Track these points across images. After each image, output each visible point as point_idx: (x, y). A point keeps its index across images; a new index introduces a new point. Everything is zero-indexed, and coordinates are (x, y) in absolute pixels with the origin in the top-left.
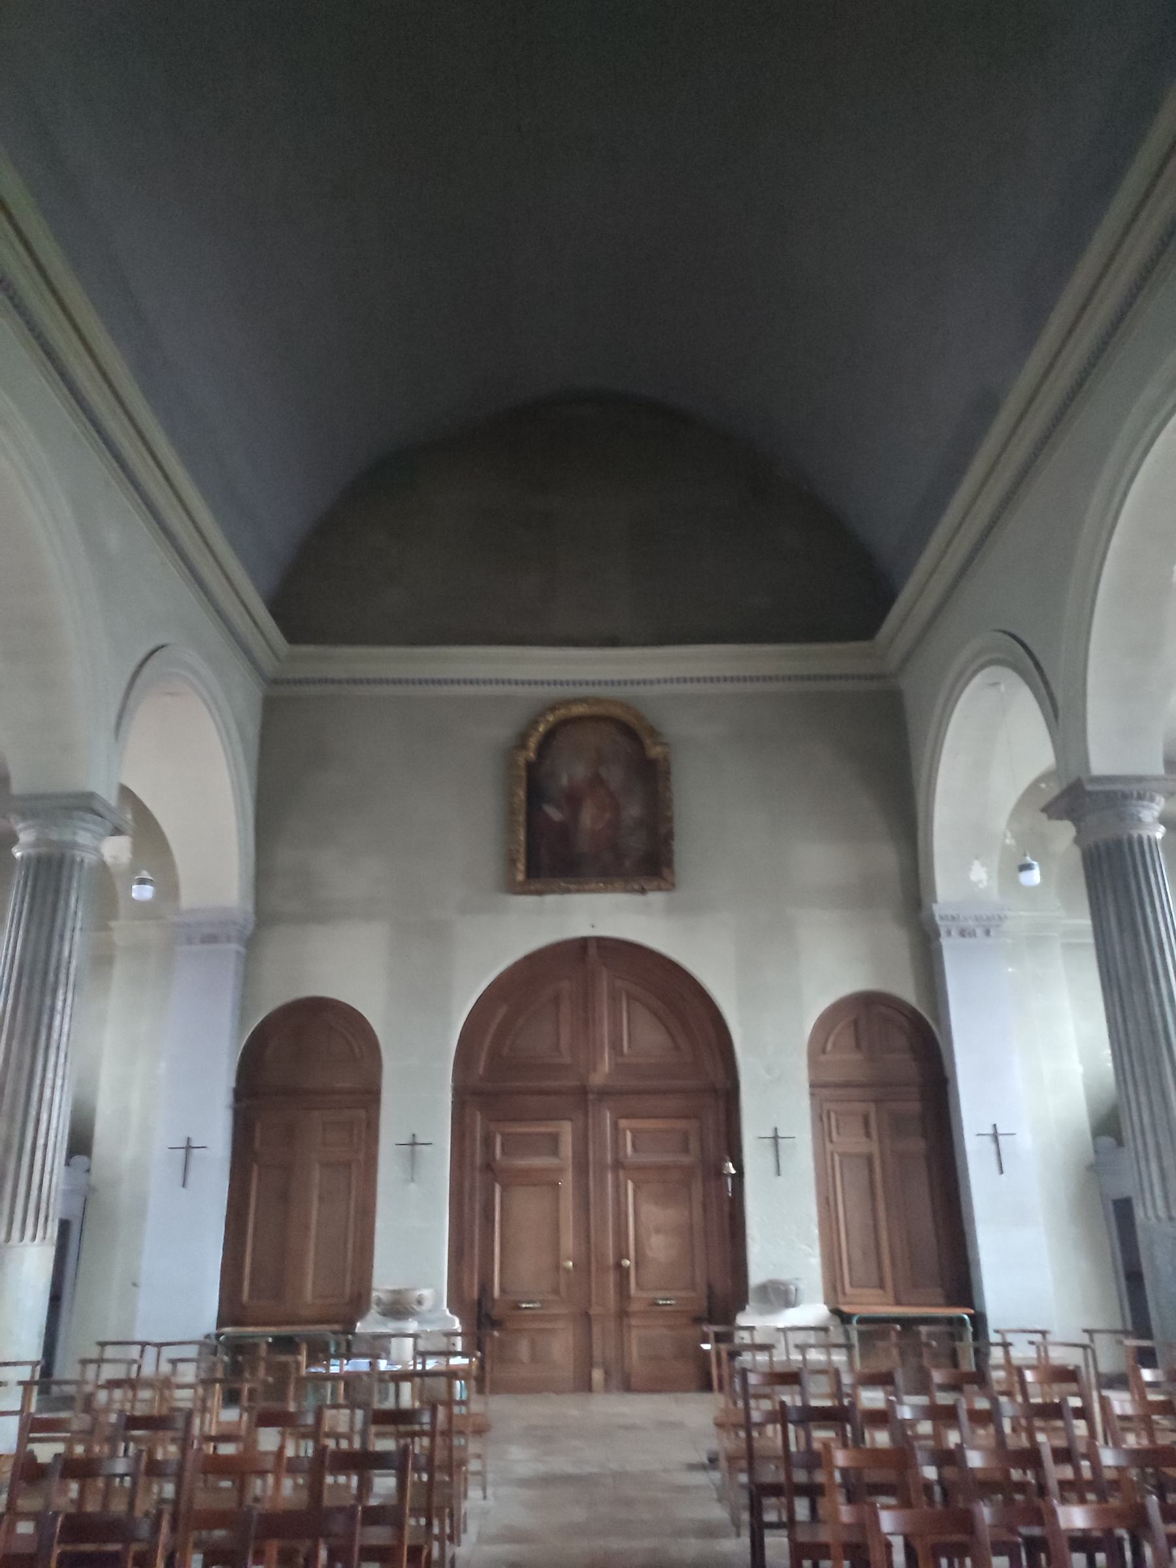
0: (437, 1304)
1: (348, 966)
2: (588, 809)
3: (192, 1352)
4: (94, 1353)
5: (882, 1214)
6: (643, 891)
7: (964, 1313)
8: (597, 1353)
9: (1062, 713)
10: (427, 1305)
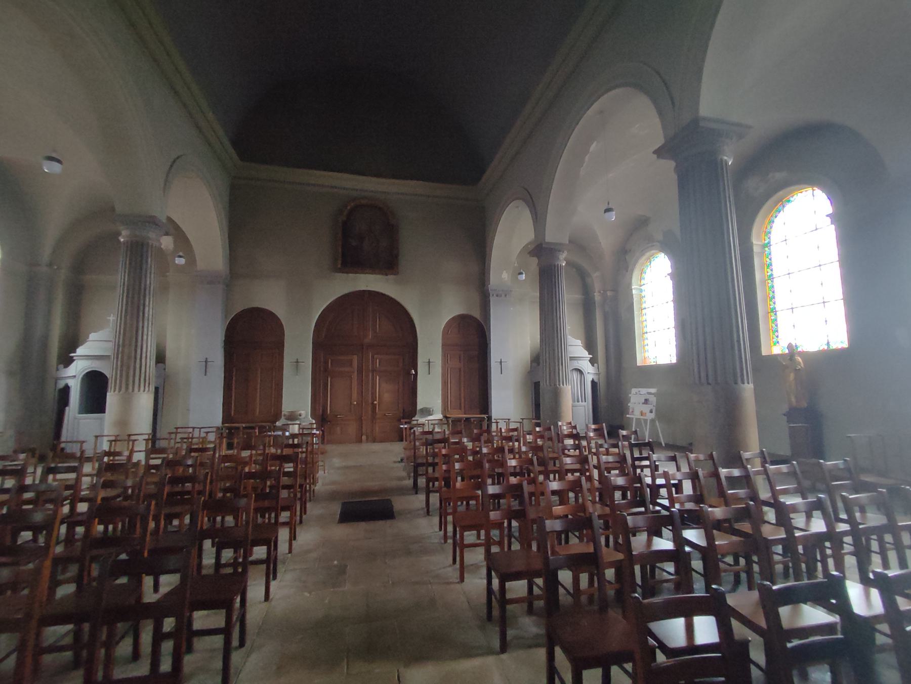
0: (307, 415)
1: (270, 297)
2: (364, 241)
3: (214, 430)
4: (175, 430)
5: (462, 378)
6: (387, 275)
7: (485, 416)
8: (364, 431)
9: (539, 219)
10: (303, 416)
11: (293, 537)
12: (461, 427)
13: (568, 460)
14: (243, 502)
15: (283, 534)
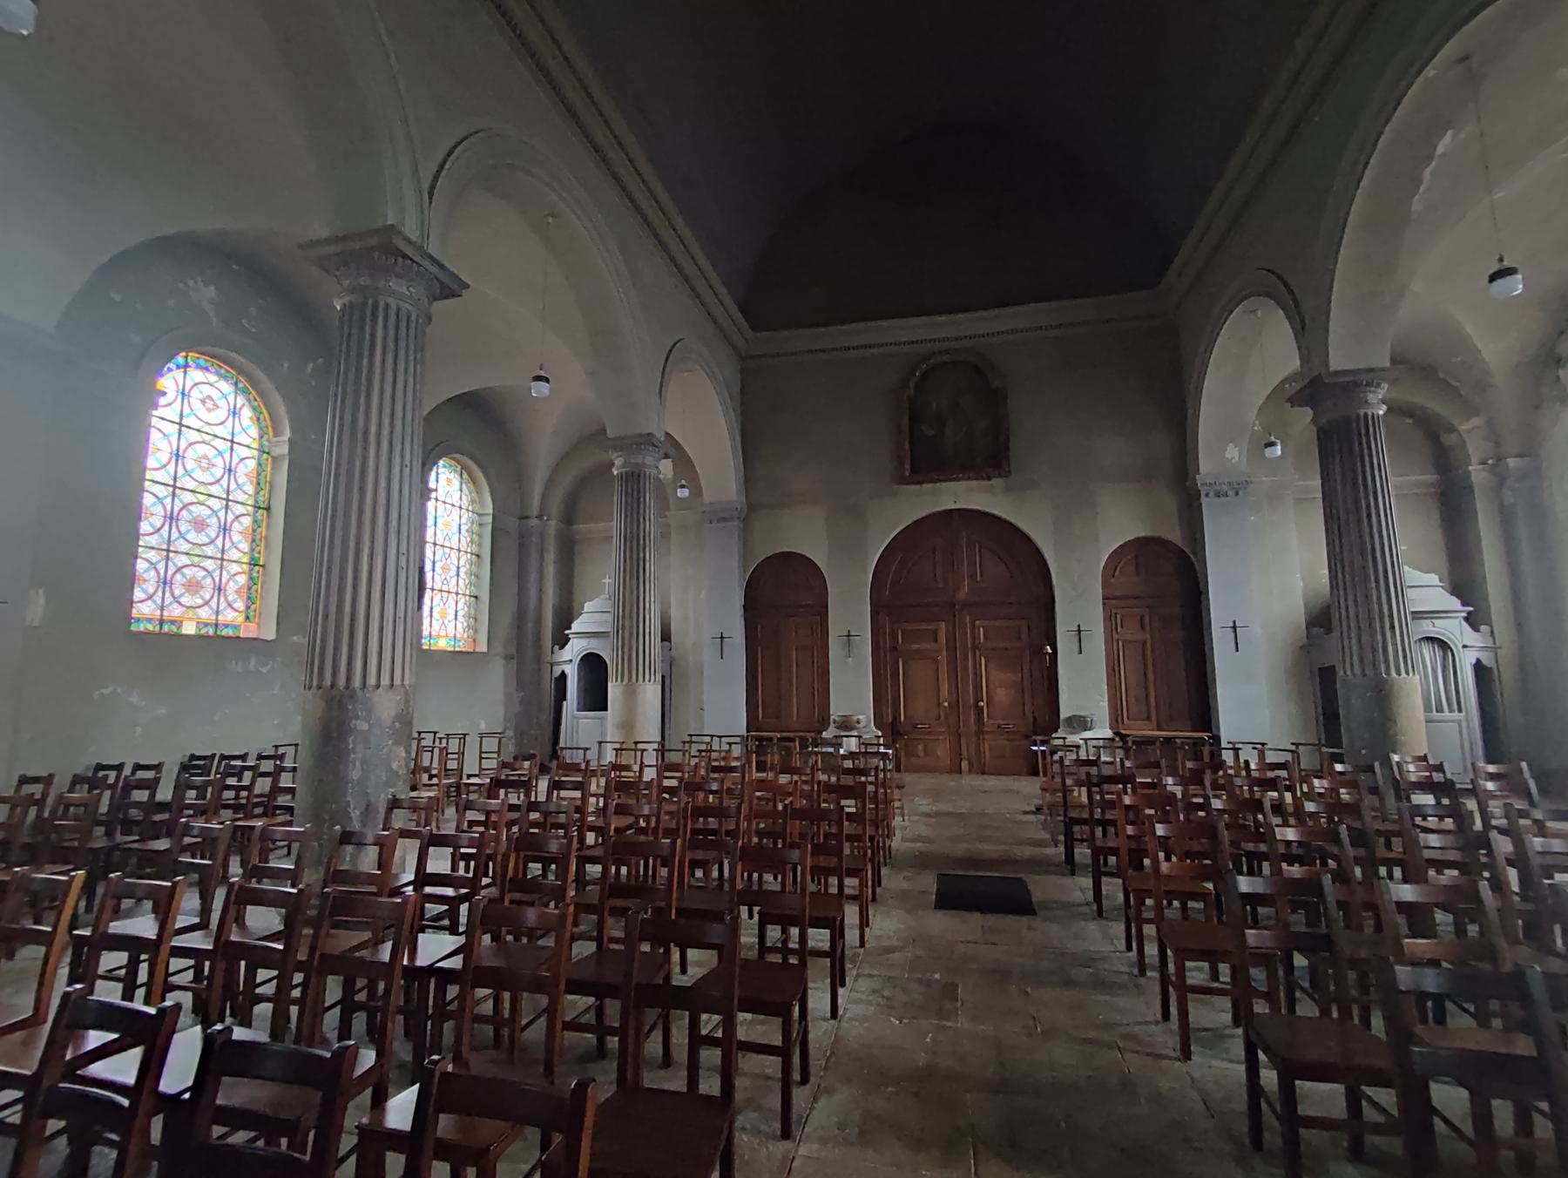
1: (805, 534)
2: (955, 424)
6: (989, 479)
7: (1205, 735)
9: (1309, 328)
11: (864, 922)
12: (1156, 753)
13: (1434, 840)
14: (795, 855)
15: (851, 914)
